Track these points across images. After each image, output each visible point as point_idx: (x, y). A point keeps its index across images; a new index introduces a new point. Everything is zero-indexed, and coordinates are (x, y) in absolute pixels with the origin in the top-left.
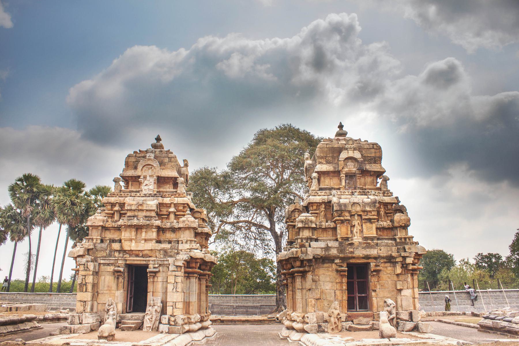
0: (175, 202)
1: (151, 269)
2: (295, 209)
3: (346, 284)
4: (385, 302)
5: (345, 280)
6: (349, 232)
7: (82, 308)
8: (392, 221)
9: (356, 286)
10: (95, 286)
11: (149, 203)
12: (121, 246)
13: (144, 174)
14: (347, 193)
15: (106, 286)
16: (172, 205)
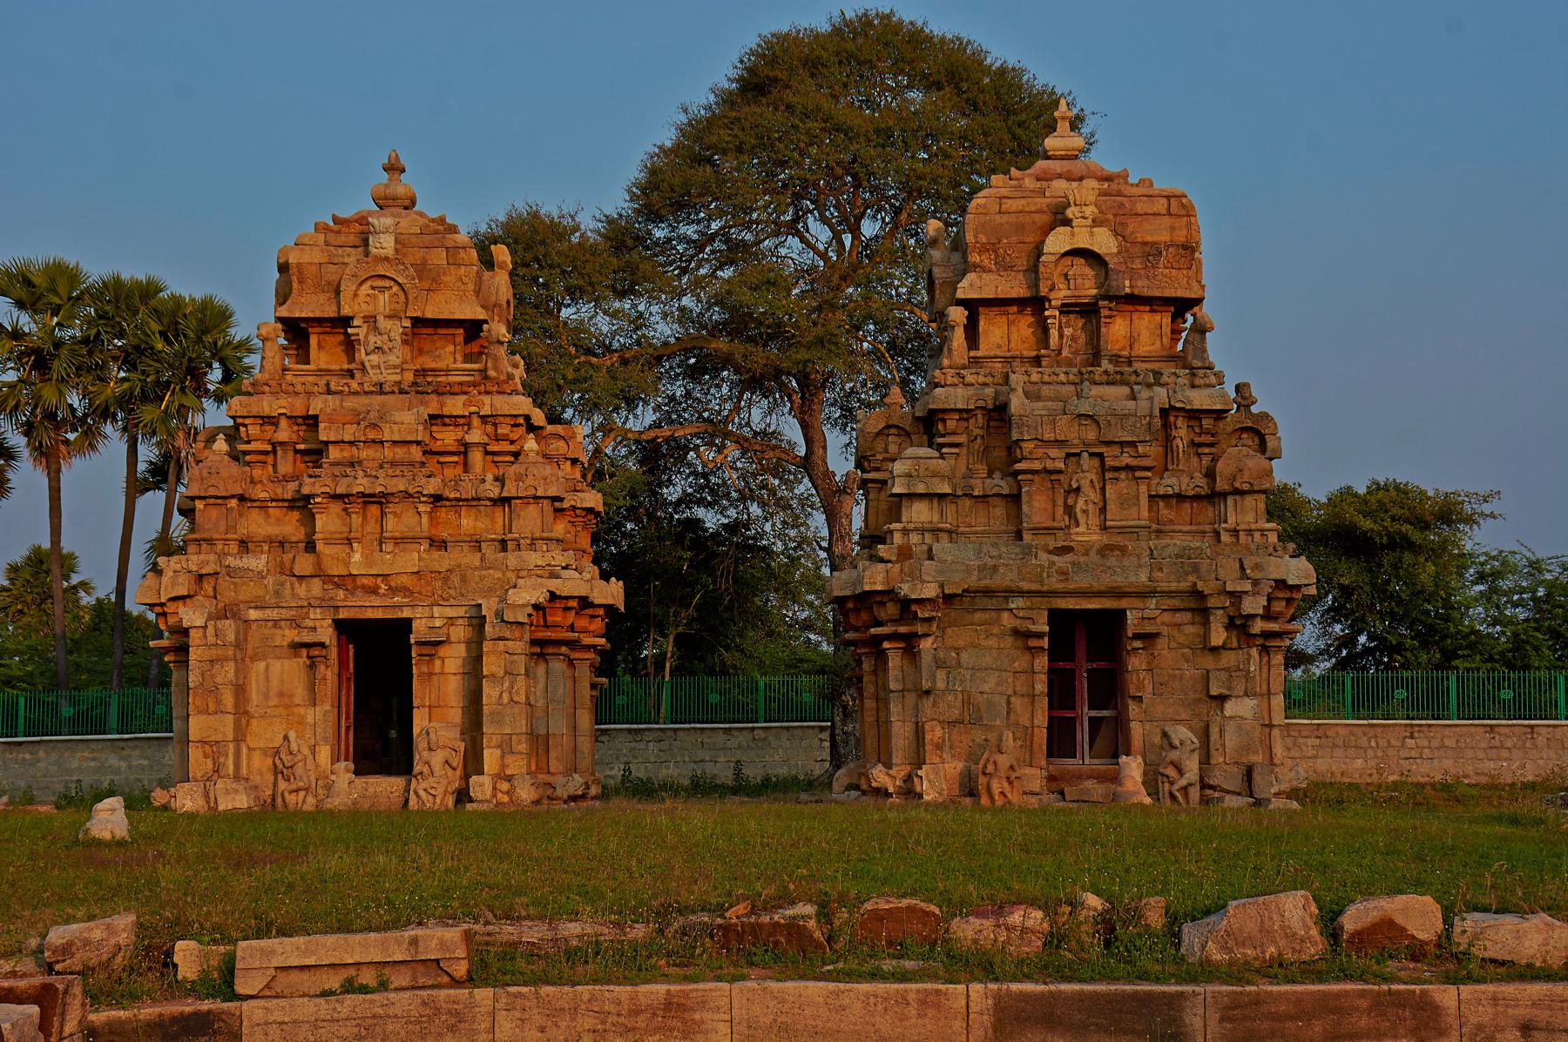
0: (486, 411)
1: (419, 630)
2: (888, 427)
3: (1044, 677)
4: (1165, 735)
5: (1042, 662)
6: (1060, 511)
7: (209, 762)
8: (1210, 474)
9: (1083, 685)
10: (240, 691)
11: (398, 417)
12: (319, 564)
13: (367, 309)
14: (1062, 377)
15: (272, 693)
16: (476, 421)
